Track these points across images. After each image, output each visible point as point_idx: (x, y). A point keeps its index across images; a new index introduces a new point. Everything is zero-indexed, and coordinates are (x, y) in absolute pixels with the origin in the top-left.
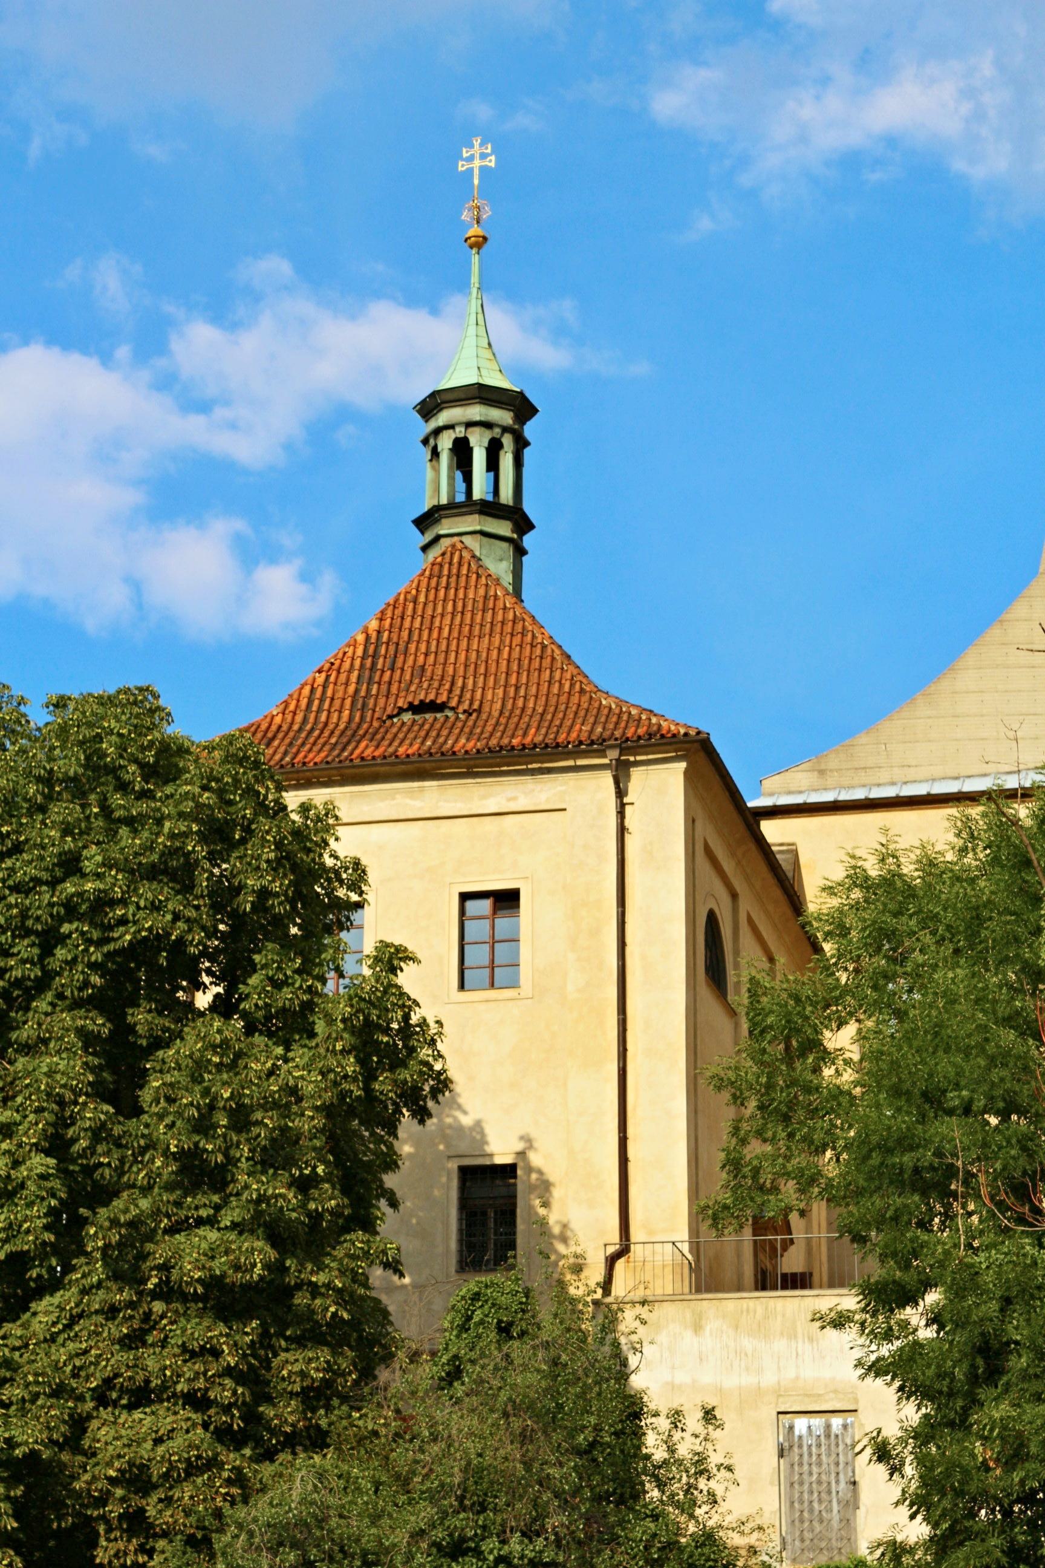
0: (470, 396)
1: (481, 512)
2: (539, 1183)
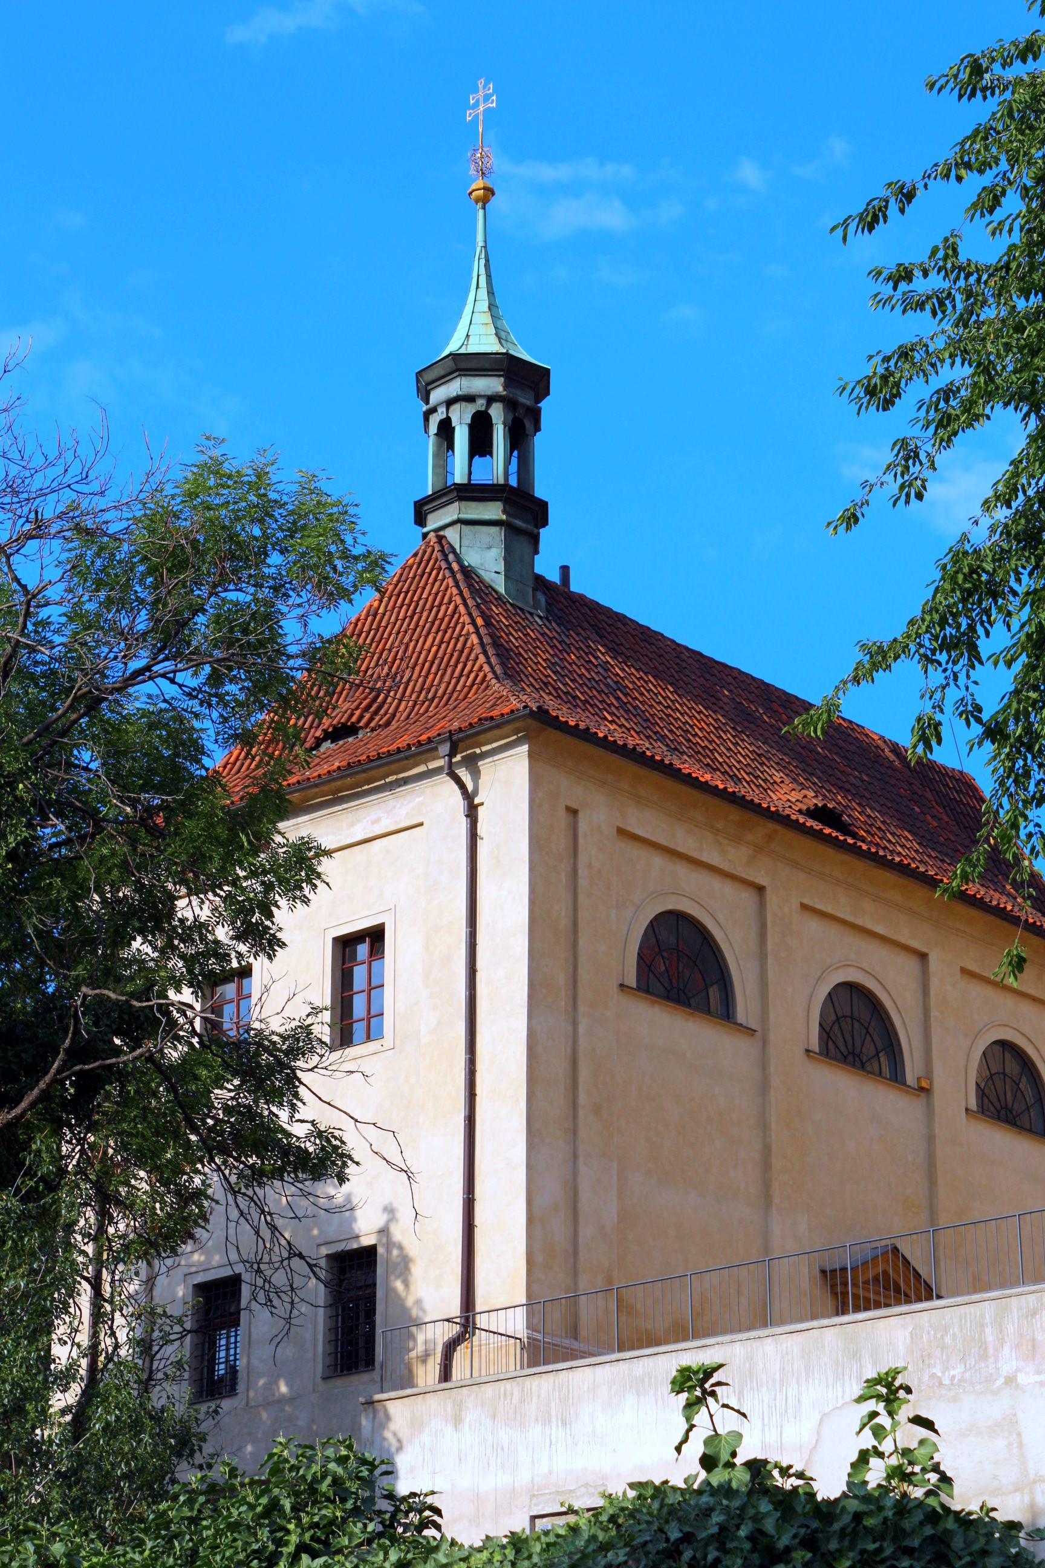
0: (448, 370)
1: (461, 499)
2: (399, 1260)
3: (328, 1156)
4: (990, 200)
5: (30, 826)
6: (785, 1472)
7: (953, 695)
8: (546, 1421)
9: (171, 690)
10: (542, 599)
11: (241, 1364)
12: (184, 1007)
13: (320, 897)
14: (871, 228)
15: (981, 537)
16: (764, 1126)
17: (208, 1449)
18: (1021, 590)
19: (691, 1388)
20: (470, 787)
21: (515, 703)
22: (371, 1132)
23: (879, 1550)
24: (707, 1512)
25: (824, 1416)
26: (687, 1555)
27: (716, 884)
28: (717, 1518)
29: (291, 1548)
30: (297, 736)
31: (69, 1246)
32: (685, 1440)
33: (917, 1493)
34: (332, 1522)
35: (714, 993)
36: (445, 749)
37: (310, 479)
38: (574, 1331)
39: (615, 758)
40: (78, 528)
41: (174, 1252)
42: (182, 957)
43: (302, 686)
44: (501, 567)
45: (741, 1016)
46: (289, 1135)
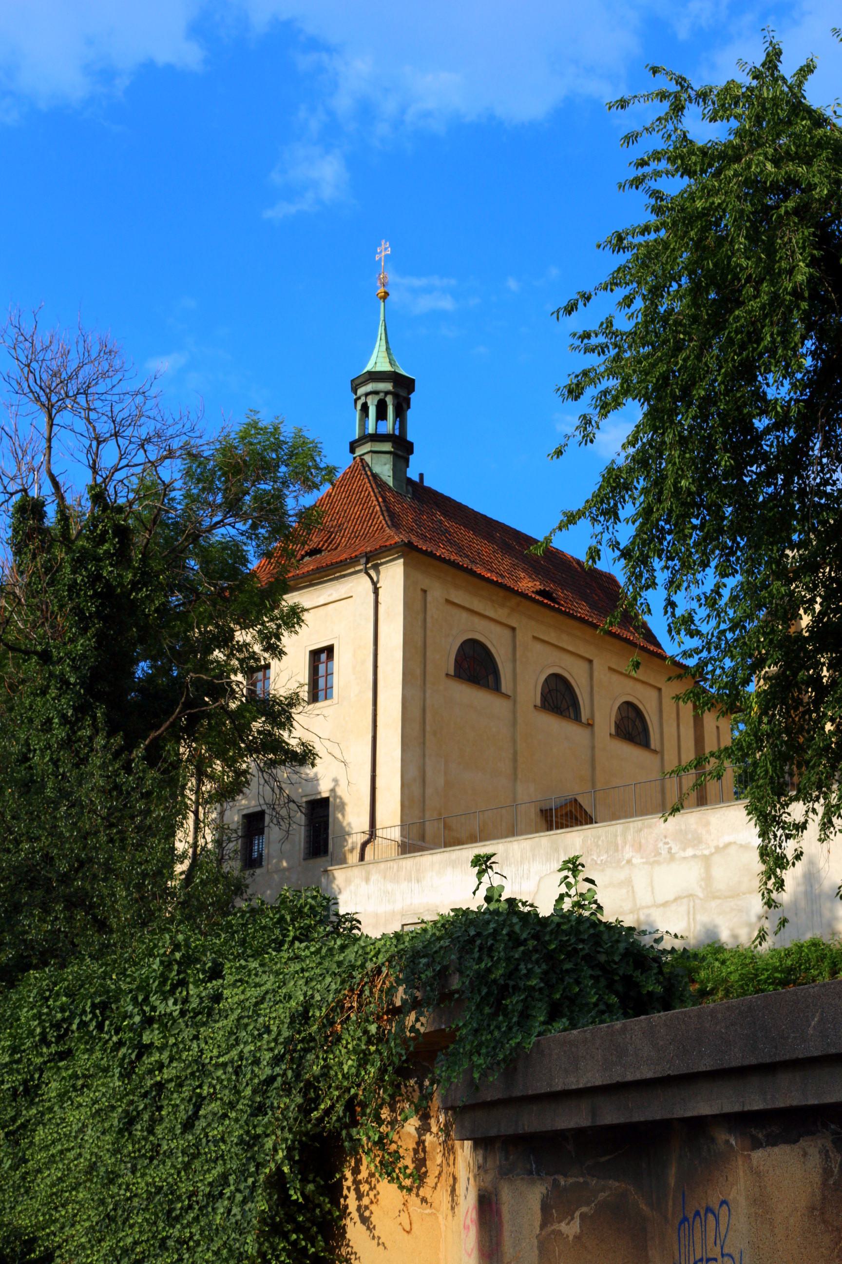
3: (306, 754)
4: (628, 301)
5: (166, 596)
6: (524, 904)
7: (606, 536)
8: (409, 880)
9: (233, 532)
10: (410, 489)
11: (265, 852)
12: (238, 683)
13: (303, 631)
14: (570, 314)
15: (621, 461)
16: (514, 742)
17: (249, 891)
18: (639, 487)
19: (481, 865)
20: (375, 579)
21: (397, 539)
22: (327, 743)
23: (568, 940)
24: (488, 922)
25: (541, 878)
26: (478, 942)
27: (493, 627)
28: (492, 925)
29: (290, 938)
30: (293, 554)
31: (184, 796)
32: (477, 889)
33: (587, 914)
34: (310, 926)
35: (491, 678)
36: (363, 561)
37: (298, 434)
38: (423, 838)
39: (445, 566)
40: (189, 454)
41: (234, 800)
42: (238, 659)
43: (295, 530)
44: (391, 474)
45: (504, 689)
46: (288, 744)
